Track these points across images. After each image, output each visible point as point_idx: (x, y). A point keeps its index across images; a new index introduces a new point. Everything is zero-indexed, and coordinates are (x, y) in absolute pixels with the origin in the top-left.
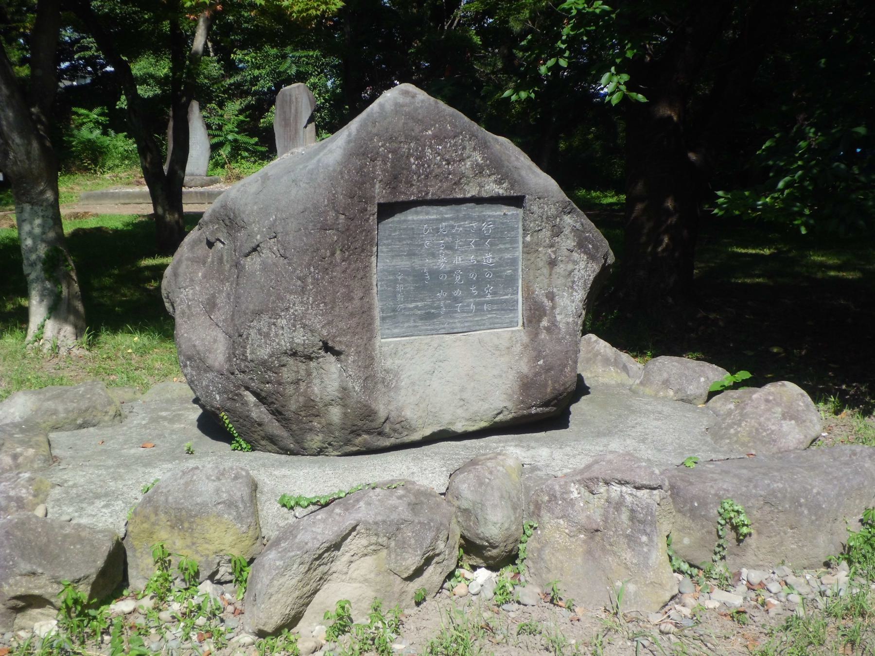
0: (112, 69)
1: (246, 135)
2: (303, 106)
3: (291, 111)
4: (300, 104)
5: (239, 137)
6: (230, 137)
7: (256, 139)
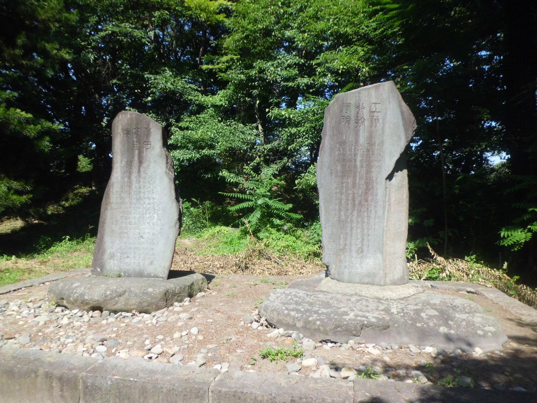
0: (75, 79)
1: (280, 201)
2: (387, 130)
3: (357, 142)
4: (379, 125)
5: (270, 202)
6: (260, 202)
7: (291, 206)
